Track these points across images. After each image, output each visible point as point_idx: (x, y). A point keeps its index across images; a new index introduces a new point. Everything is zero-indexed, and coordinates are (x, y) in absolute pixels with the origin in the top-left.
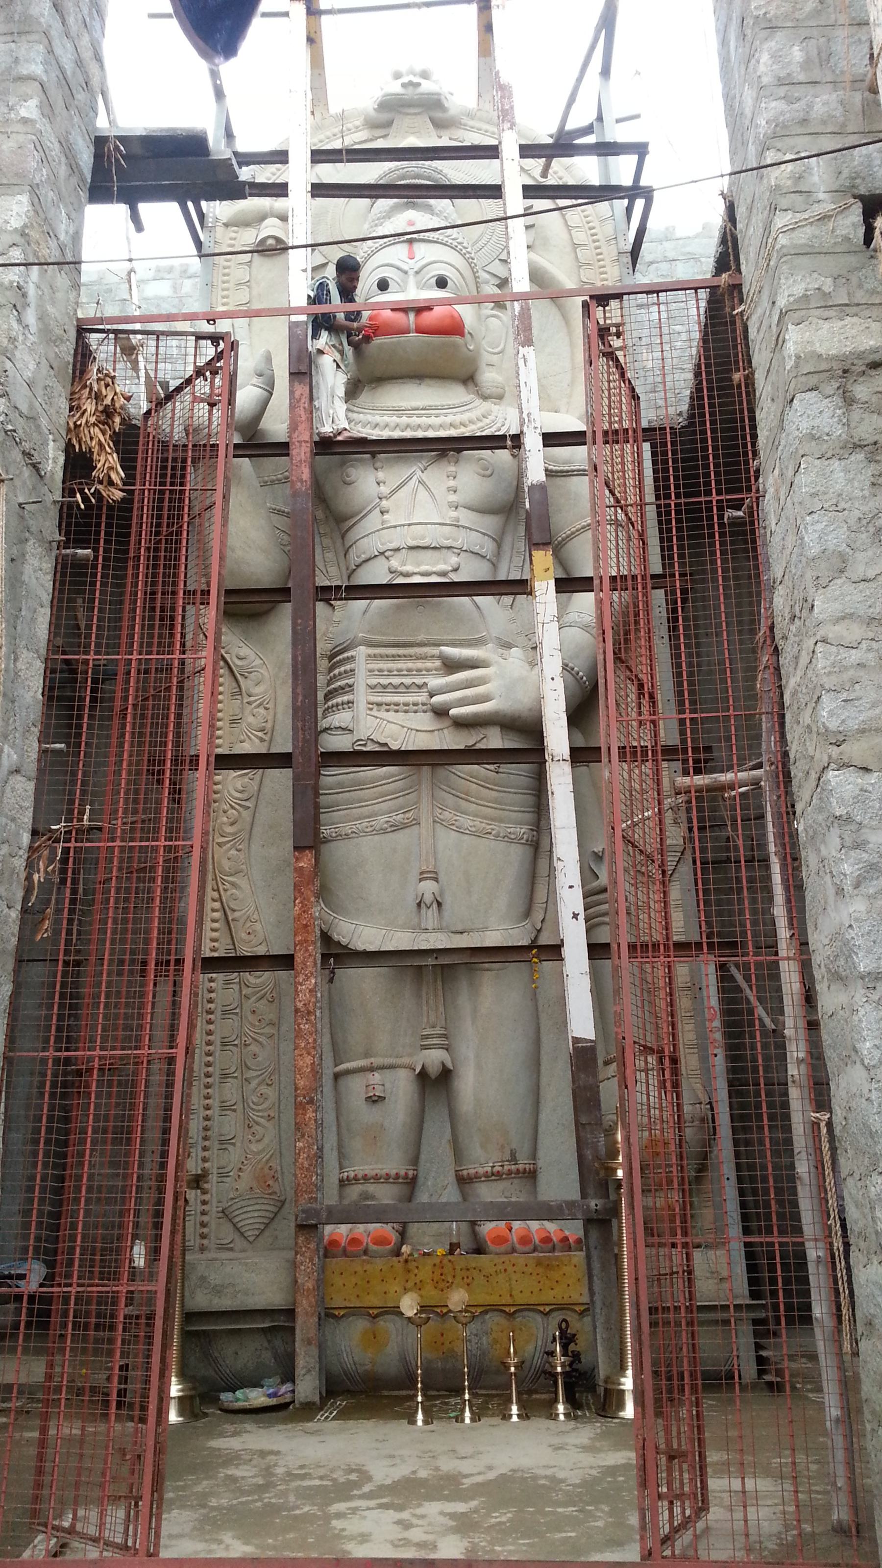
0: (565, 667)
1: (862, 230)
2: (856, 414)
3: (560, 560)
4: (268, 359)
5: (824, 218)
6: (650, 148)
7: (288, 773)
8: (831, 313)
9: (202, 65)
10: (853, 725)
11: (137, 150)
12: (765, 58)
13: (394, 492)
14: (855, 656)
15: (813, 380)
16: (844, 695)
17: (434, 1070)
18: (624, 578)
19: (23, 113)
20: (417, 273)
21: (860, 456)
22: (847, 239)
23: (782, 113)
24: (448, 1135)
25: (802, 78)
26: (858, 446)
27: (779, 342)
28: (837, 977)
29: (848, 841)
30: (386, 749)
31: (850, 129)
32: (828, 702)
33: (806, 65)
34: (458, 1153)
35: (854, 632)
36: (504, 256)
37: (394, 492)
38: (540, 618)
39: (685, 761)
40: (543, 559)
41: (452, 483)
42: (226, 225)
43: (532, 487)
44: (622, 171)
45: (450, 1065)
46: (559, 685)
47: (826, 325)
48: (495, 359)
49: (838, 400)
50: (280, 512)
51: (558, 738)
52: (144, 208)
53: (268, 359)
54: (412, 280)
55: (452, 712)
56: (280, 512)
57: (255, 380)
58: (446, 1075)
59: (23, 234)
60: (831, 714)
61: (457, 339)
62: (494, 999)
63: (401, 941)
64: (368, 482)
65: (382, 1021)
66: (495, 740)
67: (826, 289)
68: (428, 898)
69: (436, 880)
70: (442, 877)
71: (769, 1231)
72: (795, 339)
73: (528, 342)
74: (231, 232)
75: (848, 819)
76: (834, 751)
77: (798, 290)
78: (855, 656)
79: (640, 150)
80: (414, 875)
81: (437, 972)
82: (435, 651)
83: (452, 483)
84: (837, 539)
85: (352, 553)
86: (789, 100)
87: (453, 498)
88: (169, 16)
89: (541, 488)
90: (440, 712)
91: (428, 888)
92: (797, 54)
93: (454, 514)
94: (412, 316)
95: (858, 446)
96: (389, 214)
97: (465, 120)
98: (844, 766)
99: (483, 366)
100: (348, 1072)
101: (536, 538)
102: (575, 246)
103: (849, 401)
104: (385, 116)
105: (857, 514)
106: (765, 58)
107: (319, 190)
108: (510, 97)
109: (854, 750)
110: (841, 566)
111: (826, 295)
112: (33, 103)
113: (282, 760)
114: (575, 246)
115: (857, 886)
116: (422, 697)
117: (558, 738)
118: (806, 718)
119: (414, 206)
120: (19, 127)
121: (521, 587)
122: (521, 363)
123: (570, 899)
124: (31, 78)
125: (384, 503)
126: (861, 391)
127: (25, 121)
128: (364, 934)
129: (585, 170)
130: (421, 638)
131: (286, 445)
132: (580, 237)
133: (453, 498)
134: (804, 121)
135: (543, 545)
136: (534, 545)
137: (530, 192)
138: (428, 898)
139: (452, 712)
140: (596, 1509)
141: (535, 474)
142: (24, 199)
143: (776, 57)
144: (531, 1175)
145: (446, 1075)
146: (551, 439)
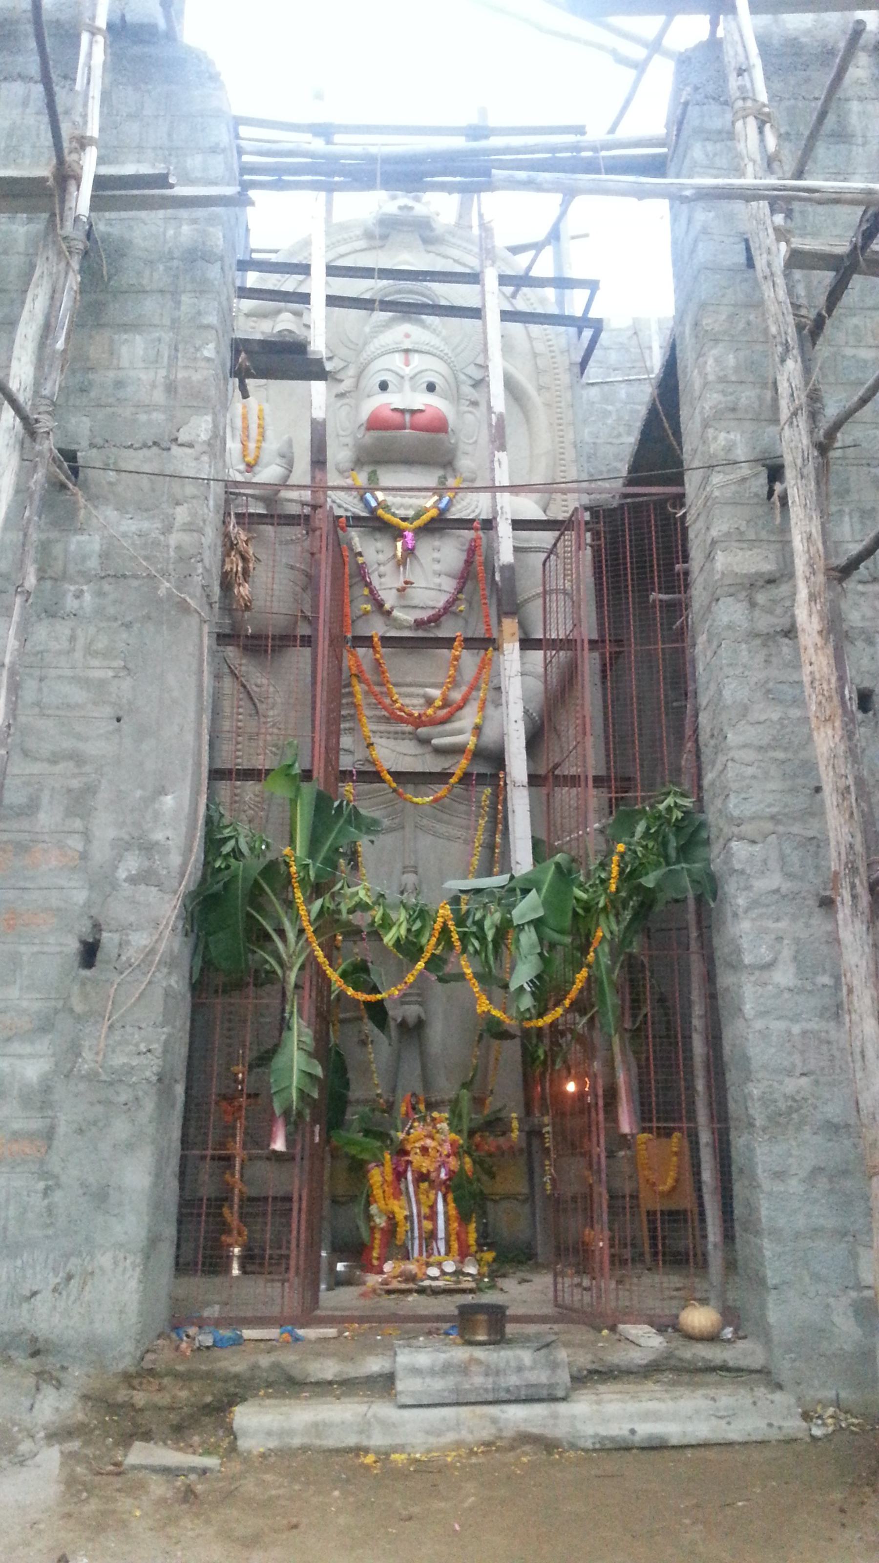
0: (526, 712)
1: (766, 489)
2: (757, 613)
3: (522, 626)
4: (290, 444)
5: (744, 480)
6: (601, 285)
8: (745, 545)
10: (748, 814)
11: (257, 348)
12: (710, 362)
14: (750, 771)
15: (732, 590)
16: (743, 795)
17: (411, 1021)
18: (569, 641)
19: (206, 353)
20: (412, 378)
21: (758, 641)
22: (756, 495)
23: (720, 402)
24: (418, 1072)
25: (734, 379)
26: (758, 635)
27: (709, 557)
29: (742, 885)
31: (762, 417)
32: (733, 801)
33: (737, 370)
34: (426, 1081)
35: (749, 755)
36: (480, 361)
38: (507, 673)
39: (610, 787)
40: (510, 625)
42: (247, 315)
43: (503, 568)
44: (576, 303)
45: (423, 1016)
47: (741, 553)
48: (469, 449)
49: (745, 604)
50: (292, 568)
51: (518, 765)
52: (250, 383)
53: (290, 444)
54: (407, 385)
55: (434, 741)
56: (292, 568)
57: (279, 460)
58: (420, 1024)
59: (209, 445)
60: (735, 806)
61: (441, 435)
67: (742, 529)
68: (410, 887)
69: (416, 873)
70: (420, 870)
71: (680, 1119)
72: (721, 560)
73: (502, 448)
74: (251, 322)
75: (742, 872)
76: (736, 830)
77: (725, 528)
78: (750, 771)
79: (593, 286)
80: (399, 866)
82: (421, 691)
83: (436, 555)
84: (743, 694)
86: (724, 393)
87: (437, 567)
89: (509, 569)
91: (410, 879)
92: (731, 360)
93: (437, 580)
94: (408, 417)
95: (758, 635)
96: (387, 325)
97: (448, 237)
98: (741, 838)
99: (459, 453)
101: (506, 608)
102: (535, 355)
103: (753, 604)
105: (755, 679)
106: (710, 362)
107: (333, 301)
108: (492, 237)
109: (747, 829)
110: (745, 710)
111: (742, 533)
112: (211, 346)
114: (535, 355)
115: (746, 912)
117: (518, 765)
118: (718, 803)
119: (409, 320)
120: (203, 364)
121: (487, 644)
122: (496, 464)
124: (208, 327)
126: (761, 598)
127: (208, 360)
129: (546, 300)
130: (409, 679)
132: (540, 347)
133: (437, 567)
134: (734, 410)
135: (511, 614)
136: (503, 613)
137: (507, 316)
138: (410, 887)
139: (434, 741)
141: (506, 555)
142: (209, 418)
143: (717, 360)
145: (420, 1024)
146: (518, 525)
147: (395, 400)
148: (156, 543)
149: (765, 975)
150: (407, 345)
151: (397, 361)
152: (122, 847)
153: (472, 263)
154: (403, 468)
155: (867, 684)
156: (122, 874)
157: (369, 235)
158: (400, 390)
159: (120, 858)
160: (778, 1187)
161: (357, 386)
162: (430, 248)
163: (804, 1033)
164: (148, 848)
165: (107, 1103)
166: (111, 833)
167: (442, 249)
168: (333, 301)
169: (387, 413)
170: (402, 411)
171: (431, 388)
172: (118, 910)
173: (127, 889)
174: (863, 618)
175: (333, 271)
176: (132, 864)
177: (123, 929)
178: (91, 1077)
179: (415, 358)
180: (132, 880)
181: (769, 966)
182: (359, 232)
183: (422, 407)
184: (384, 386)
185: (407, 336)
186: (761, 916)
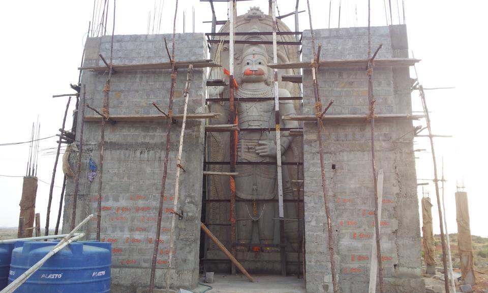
7: (229, 166)
9: (406, 23)
13: (249, 108)
14: (309, 182)
28: (306, 159)
30: (247, 161)
37: (249, 108)
41: (261, 107)
46: (280, 152)
62: (265, 209)
63: (249, 197)
64: (245, 106)
65: (245, 209)
66: (268, 160)
81: (256, 203)
85: (241, 120)
88: (425, 89)
90: (258, 154)
91: (255, 187)
100: (239, 220)
104: (249, 19)
113: (228, 163)
116: (254, 150)
123: (281, 192)
125: (248, 111)
128: (243, 196)
131: (229, 99)
140: (258, 142)
144: (273, 240)
147: (249, 67)
148: (191, 134)
149: (309, 223)
150: (254, 53)
151: (251, 57)
152: (186, 197)
153: (269, 29)
154: (254, 83)
155: (334, 163)
156: (186, 202)
157: (245, 20)
158: (252, 64)
159: (186, 198)
160: (309, 264)
161: (242, 62)
162: (262, 22)
163: (317, 235)
164: (190, 196)
165: (185, 244)
166: (184, 194)
167: (264, 22)
168: (236, 42)
169: (249, 72)
170: (252, 71)
171: (260, 63)
172: (186, 208)
173: (187, 205)
174: (335, 149)
175: (237, 34)
176: (188, 200)
177: (187, 212)
178: (182, 240)
179: (256, 56)
180: (188, 203)
181: (310, 222)
182: (243, 19)
183: (257, 69)
184: (248, 64)
185: (254, 50)
186: (309, 212)
